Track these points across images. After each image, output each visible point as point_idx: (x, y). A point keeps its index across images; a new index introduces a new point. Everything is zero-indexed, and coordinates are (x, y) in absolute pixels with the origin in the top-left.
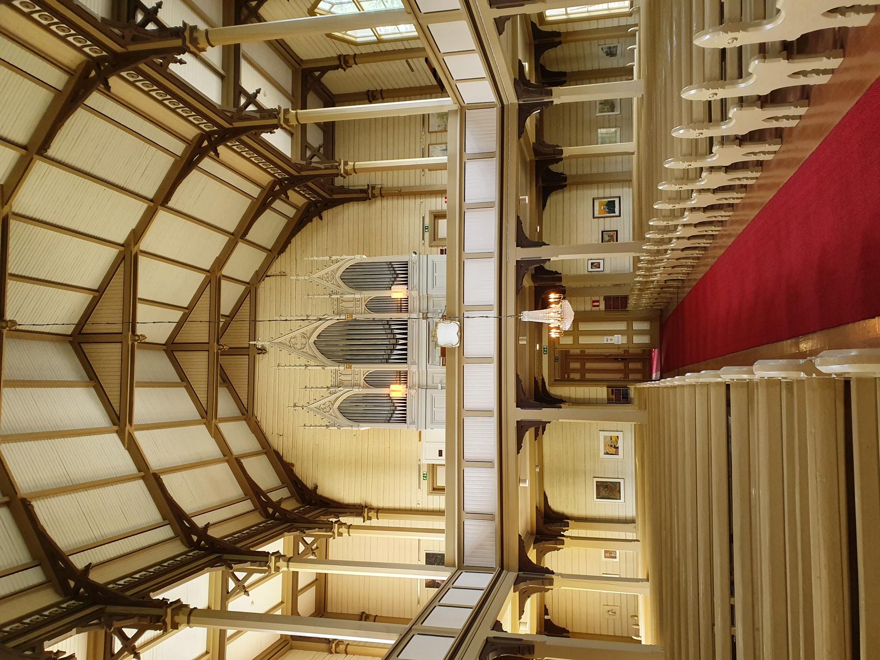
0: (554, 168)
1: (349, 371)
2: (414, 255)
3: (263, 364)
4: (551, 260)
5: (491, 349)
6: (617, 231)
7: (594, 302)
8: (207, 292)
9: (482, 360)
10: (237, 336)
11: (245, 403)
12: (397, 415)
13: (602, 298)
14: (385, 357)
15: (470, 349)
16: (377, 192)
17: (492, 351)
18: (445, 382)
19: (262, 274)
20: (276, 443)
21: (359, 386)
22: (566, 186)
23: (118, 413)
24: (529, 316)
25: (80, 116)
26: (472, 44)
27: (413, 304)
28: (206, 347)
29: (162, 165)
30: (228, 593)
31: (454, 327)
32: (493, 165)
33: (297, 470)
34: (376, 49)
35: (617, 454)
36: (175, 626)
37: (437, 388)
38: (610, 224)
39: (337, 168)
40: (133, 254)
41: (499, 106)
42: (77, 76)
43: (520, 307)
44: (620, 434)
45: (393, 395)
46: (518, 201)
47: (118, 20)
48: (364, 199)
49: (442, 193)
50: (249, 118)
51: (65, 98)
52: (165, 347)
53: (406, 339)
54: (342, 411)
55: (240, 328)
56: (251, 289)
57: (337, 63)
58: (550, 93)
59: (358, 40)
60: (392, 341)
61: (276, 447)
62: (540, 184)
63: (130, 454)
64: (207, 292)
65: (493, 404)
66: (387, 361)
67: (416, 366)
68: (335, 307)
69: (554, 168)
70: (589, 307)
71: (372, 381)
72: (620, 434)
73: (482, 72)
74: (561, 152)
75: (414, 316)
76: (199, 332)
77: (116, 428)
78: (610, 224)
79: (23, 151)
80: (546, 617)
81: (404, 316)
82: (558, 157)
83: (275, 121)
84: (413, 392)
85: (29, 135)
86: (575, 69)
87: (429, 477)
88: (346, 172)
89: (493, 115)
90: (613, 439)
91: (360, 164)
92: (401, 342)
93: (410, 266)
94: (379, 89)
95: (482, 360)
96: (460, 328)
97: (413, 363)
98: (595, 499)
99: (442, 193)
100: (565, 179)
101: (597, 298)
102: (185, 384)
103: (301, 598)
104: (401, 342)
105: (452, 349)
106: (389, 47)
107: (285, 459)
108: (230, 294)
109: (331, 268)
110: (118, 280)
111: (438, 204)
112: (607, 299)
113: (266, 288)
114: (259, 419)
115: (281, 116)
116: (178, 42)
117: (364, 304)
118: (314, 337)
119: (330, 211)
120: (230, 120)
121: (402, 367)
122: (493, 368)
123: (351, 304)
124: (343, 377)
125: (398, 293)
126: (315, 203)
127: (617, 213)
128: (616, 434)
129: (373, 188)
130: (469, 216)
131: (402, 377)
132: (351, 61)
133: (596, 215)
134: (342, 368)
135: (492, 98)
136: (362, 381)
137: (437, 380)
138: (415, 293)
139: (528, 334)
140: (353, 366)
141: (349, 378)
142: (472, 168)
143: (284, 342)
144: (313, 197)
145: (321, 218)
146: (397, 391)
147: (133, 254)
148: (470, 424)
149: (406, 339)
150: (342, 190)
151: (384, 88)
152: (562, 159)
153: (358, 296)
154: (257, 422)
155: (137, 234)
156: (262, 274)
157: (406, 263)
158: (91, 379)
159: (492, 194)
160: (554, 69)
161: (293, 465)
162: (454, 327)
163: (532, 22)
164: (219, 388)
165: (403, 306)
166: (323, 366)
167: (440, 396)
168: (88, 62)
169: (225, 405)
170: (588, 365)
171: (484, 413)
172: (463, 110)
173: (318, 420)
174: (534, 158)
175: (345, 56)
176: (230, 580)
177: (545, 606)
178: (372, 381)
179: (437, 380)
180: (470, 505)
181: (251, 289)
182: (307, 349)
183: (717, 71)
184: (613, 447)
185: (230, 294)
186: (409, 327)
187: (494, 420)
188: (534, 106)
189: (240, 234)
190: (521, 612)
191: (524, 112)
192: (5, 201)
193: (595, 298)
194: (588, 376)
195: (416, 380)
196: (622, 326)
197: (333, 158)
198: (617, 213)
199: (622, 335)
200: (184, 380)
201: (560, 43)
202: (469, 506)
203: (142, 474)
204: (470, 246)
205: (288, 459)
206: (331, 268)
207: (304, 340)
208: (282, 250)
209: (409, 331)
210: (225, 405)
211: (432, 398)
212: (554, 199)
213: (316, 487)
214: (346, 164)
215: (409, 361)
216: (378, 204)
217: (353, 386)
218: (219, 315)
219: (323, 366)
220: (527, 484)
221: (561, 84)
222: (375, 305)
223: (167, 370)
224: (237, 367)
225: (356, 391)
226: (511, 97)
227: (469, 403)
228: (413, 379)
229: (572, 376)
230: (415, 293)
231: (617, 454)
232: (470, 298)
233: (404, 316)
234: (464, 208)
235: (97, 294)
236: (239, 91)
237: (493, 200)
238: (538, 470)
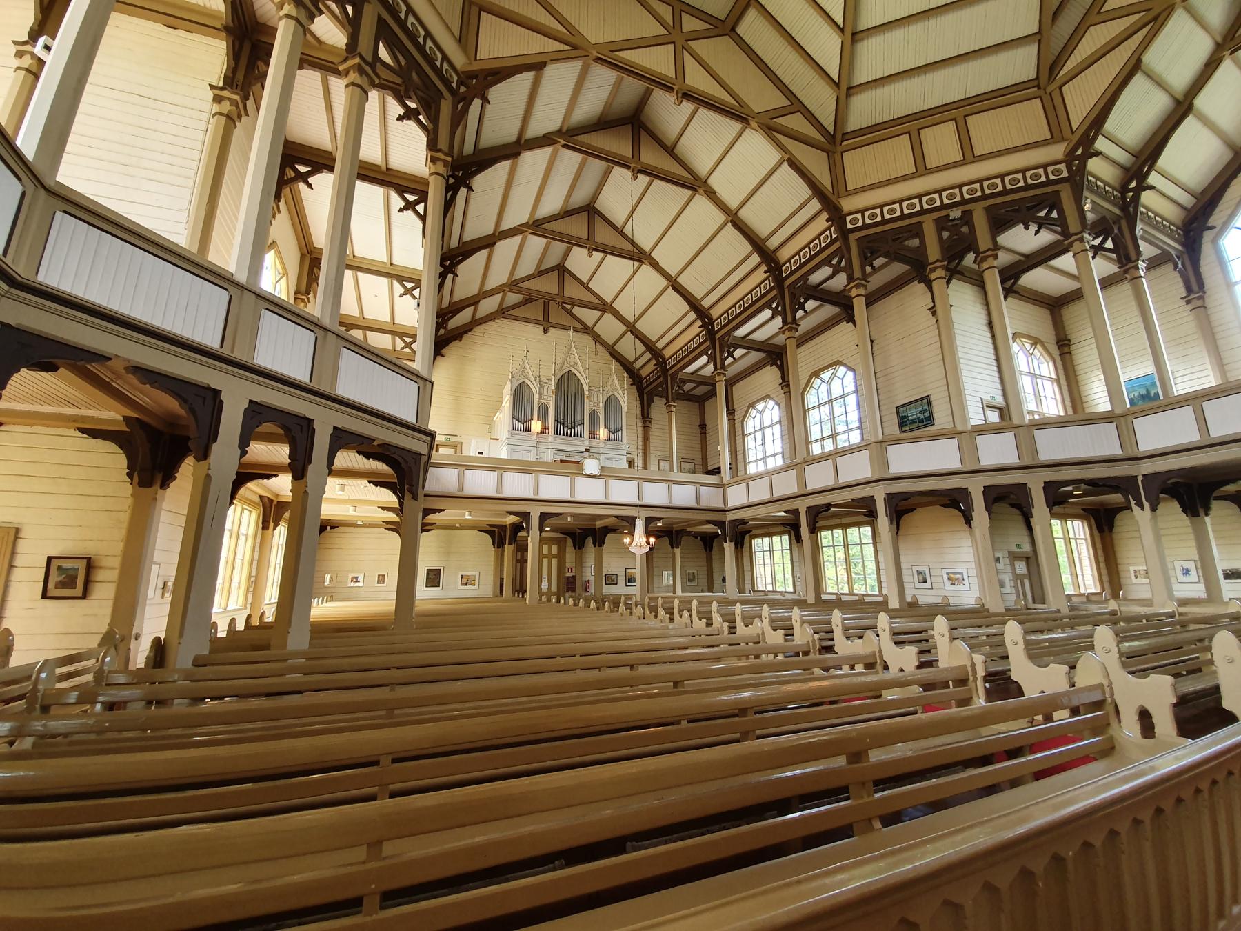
0: (589, 541)
1: (550, 392)
2: (628, 446)
3: (537, 330)
4: (725, 544)
5: (580, 497)
6: (45, 596)
7: (572, 569)
8: (597, 301)
9: (573, 490)
10: (556, 315)
11: (509, 313)
12: (518, 424)
13: (574, 574)
14: (566, 423)
15: (580, 482)
16: (648, 424)
17: (579, 498)
18: (541, 460)
19: (597, 339)
20: (478, 330)
21: (540, 398)
22: (575, 549)
23: (540, 226)
24: (639, 525)
25: (748, 248)
26: (777, 494)
27: (594, 443)
28: (561, 294)
29: (698, 292)
30: (403, 281)
31: (596, 472)
32: (693, 504)
33: (456, 343)
34: (738, 433)
35: (462, 584)
36: (1188, 302)
37: (537, 455)
38: (622, 580)
39: (672, 401)
40: (644, 261)
41: (726, 509)
42: (773, 255)
43: (649, 521)
44: (476, 587)
45: (533, 422)
46: (659, 519)
47: (806, 288)
48: (643, 415)
49: (645, 467)
50: (722, 353)
51: (761, 244)
52: (562, 265)
53: (571, 435)
54: (522, 385)
55: (564, 319)
56: (586, 330)
57: (730, 408)
58: (731, 541)
59: (745, 423)
60: (569, 426)
61: (474, 330)
62: (579, 531)
63: (266, 168)
64: (597, 301)
65: (542, 496)
66: (556, 420)
67: (552, 441)
68: (594, 388)
69: (589, 541)
70: (568, 565)
71: (543, 409)
72: (476, 587)
73: (753, 500)
74: (677, 548)
75: (587, 443)
76: (572, 291)
77: (531, 223)
78: (622, 580)
79: (734, 213)
80: (329, 528)
81: (586, 435)
82: (674, 546)
83: (719, 367)
84: (534, 437)
85: (742, 218)
86: (713, 557)
87: (447, 443)
88: (670, 406)
89: (720, 505)
90: (473, 582)
91: (673, 414)
92: (569, 432)
93: (619, 443)
94: (707, 432)
95: (573, 490)
96: (596, 476)
97: (555, 439)
98: (427, 568)
99: (645, 467)
100: (580, 548)
101: (574, 571)
102: (536, 273)
103: (360, 332)
104: (569, 432)
105: (581, 468)
106: (739, 441)
107: (465, 335)
108: (588, 316)
109: (531, 376)
110: (627, 246)
111: (639, 463)
112: (574, 577)
113: (587, 340)
114: (496, 321)
115: (722, 371)
116: (789, 320)
117: (545, 402)
118: (574, 371)
119: (636, 391)
120: (721, 339)
121: (551, 430)
122: (567, 497)
123: (595, 399)
124: (546, 387)
125: (603, 433)
126: (641, 382)
127: (628, 584)
128: (477, 585)
129: (650, 422)
130: (664, 486)
131: (545, 430)
132: (731, 417)
133: (628, 570)
134: (553, 388)
135: (731, 504)
136: (543, 401)
137: (542, 455)
138: (602, 444)
139: (574, 523)
140: (554, 396)
141: (545, 392)
142: (662, 487)
143: (572, 349)
144: (646, 382)
145: (632, 384)
146: (536, 426)
147: (644, 261)
148: (528, 478)
149: (571, 435)
150: (650, 401)
151: (707, 436)
152: (672, 547)
153: (601, 405)
154: (494, 319)
155: (655, 265)
156: (597, 339)
157: (621, 441)
158: (565, 212)
159: (677, 502)
160: (715, 544)
161: (460, 341)
162: (596, 472)
163: (751, 531)
164: (522, 296)
165: (593, 435)
166: (554, 375)
167: (531, 457)
168: (779, 263)
169: (513, 298)
170: (554, 561)
171: (536, 489)
172: (723, 486)
173: (517, 366)
174: (597, 527)
175: (734, 413)
176: (413, 285)
177: (338, 527)
178: (543, 409)
179: (542, 455)
180: (469, 474)
181: (586, 330)
182: (566, 365)
183: (896, 631)
184: (466, 581)
185: (588, 316)
186: (579, 438)
187: (531, 496)
188: (723, 530)
189: (632, 328)
190: (384, 509)
191: (720, 524)
192: (708, 193)
193: (574, 569)
194: (545, 561)
195: (543, 440)
196: (554, 588)
197: (678, 399)
198: (628, 584)
199: (548, 589)
200: (540, 273)
201: (706, 550)
202: (469, 473)
203: (497, 234)
204: (646, 486)
205: (465, 337)
206: (531, 376)
207: (573, 363)
208: (613, 356)
209: (572, 438)
210: (513, 298)
211: (529, 451)
212: (487, 538)
213: (443, 356)
214: (675, 406)
215: (513, 431)
216: (640, 424)
217: (540, 394)
218: (574, 305)
219: (554, 375)
220: (468, 517)
221: (736, 547)
222: (594, 415)
223: (552, 261)
224: (536, 311)
225: (536, 396)
226: (730, 517)
227: (543, 478)
228: (543, 438)
229: (519, 554)
230: (602, 444)
231: (462, 584)
232: (614, 484)
233: (586, 435)
234: (697, 485)
235: (620, 230)
236: (736, 348)
237: (503, 492)
238: (457, 525)
